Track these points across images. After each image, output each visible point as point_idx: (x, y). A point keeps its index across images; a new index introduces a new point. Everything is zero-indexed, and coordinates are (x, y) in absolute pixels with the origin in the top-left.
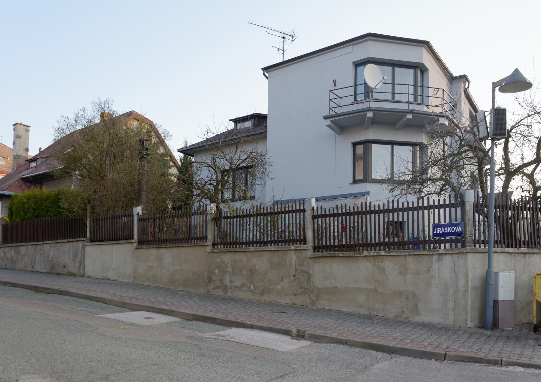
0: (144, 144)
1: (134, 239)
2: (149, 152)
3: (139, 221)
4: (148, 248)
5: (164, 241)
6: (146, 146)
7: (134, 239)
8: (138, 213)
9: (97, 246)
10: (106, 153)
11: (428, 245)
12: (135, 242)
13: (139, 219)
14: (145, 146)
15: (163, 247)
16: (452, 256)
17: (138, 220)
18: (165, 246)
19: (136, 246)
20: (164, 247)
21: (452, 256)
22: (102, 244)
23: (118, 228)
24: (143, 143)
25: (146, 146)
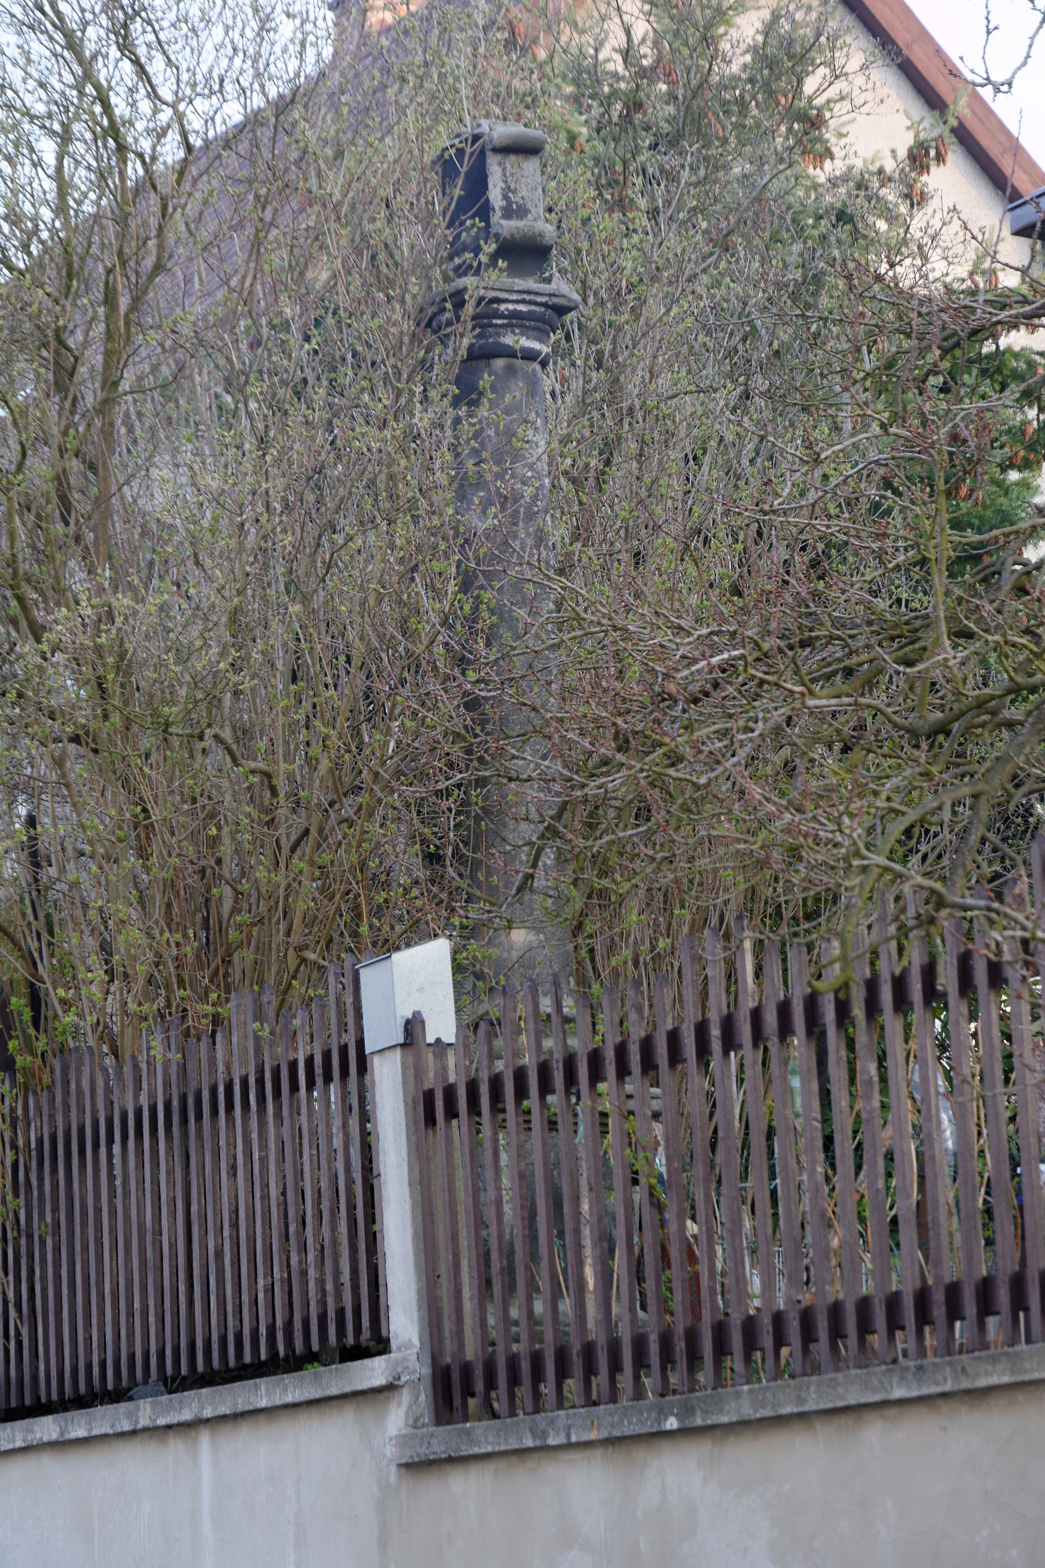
0: (495, 195)
1: (381, 1345)
2: (563, 287)
3: (430, 1120)
4: (522, 1453)
5: (750, 1343)
6: (522, 212)
7: (381, 1345)
8: (413, 1027)
9: (48, 1464)
10: (106, 363)
11: (263, 1357)
12: (391, 1388)
13: (429, 1097)
14: (508, 213)
15: (672, 1423)
16: (532, 890)
17: (410, 1107)
18: (687, 1411)
19: (402, 1441)
20: (685, 1432)
21: (532, 890)
22: (80, 1433)
23: (235, 1225)
24: (478, 182)
25: (522, 212)
